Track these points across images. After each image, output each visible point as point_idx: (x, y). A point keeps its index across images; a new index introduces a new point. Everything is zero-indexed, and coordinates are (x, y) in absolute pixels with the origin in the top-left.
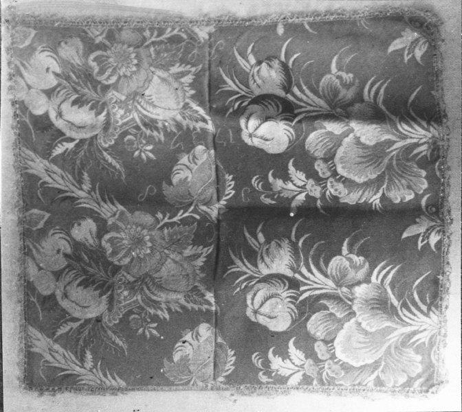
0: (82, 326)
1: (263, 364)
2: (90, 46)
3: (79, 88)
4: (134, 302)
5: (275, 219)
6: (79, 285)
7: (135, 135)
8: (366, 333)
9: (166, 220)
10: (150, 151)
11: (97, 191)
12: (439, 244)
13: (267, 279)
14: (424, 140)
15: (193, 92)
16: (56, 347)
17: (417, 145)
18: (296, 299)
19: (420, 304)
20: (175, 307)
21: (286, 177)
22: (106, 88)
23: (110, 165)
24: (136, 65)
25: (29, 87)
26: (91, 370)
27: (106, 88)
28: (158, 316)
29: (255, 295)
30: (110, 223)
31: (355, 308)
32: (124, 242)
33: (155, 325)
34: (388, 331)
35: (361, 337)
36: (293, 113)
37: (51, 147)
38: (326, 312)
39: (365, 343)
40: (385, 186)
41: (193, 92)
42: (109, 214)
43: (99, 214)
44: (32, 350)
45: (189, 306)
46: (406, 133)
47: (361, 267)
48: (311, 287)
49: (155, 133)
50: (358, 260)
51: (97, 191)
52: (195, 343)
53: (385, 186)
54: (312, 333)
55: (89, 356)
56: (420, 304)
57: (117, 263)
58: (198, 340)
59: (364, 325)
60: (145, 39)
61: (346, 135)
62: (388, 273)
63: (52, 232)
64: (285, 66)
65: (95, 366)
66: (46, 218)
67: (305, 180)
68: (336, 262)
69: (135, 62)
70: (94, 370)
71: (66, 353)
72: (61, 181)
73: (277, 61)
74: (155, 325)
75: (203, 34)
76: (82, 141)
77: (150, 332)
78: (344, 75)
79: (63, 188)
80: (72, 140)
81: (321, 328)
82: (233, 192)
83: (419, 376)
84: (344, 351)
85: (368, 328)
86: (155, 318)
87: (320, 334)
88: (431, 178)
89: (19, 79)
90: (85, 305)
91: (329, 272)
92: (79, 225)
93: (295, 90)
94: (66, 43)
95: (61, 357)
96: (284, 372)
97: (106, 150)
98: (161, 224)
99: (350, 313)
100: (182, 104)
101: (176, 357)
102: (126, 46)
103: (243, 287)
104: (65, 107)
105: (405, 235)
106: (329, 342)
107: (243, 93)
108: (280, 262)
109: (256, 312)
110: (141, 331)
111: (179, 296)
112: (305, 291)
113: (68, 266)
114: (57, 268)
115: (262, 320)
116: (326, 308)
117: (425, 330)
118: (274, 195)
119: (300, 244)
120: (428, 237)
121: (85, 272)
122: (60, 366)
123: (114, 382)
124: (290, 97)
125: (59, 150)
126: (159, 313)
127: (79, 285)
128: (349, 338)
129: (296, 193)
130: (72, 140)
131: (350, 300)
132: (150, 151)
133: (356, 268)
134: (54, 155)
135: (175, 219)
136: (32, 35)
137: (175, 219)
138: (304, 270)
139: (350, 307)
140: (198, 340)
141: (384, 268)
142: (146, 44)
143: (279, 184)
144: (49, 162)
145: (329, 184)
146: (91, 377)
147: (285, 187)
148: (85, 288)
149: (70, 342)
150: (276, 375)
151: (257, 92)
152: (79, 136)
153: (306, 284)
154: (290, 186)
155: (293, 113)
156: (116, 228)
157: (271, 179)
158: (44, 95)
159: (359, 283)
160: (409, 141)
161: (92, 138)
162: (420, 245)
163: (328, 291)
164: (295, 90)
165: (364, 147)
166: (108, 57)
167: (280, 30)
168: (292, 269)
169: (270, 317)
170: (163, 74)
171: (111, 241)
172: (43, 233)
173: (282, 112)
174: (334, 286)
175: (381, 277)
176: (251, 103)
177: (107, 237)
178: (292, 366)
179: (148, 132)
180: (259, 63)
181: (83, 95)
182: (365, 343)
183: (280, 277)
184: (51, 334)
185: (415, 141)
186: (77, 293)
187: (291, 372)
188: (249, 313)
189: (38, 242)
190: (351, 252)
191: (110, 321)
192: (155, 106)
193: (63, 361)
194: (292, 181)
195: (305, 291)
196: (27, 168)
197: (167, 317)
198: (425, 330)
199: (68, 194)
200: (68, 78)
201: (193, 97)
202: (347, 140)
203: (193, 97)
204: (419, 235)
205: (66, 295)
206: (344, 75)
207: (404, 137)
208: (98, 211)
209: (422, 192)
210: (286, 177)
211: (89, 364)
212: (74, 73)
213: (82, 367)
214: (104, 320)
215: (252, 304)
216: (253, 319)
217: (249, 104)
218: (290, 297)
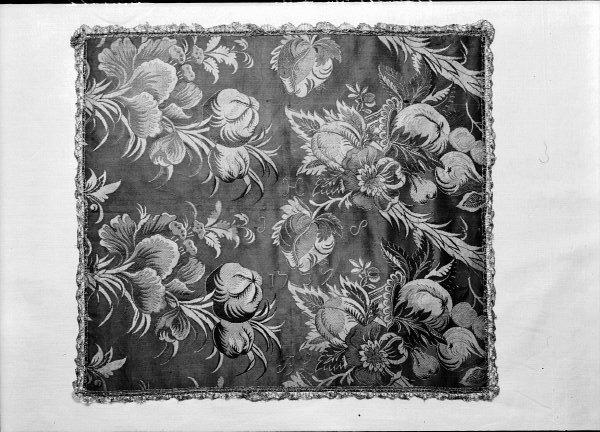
0: (424, 96)
1: (243, 57)
2: (407, 369)
3: (421, 329)
4: (370, 121)
5: (237, 194)
6: (425, 138)
7: (369, 282)
8: (149, 91)
9: (342, 200)
10: (354, 267)
11: (407, 230)
12: (87, 176)
13: (242, 141)
14: (101, 272)
15: (307, 323)
16: (448, 76)
17: (107, 268)
18: (213, 119)
19: (102, 118)
20: (330, 114)
21: (223, 241)
22: (394, 329)
23: (394, 254)
24: (361, 349)
25: (470, 329)
26: (415, 52)
27: (394, 329)
28: (347, 104)
29: (251, 122)
30: (397, 198)
31: (160, 113)
32: (384, 180)
33: (350, 96)
34: (129, 94)
35: (154, 86)
36: (215, 302)
37: (452, 271)
38: (187, 107)
39: (151, 82)
40: (136, 231)
41: (307, 323)
42: (397, 206)
43: (406, 207)
44: (477, 72)
45: (316, 117)
46: (117, 279)
47: (156, 156)
48: (199, 131)
49: (349, 284)
50: (159, 162)
51: (407, 230)
52: (311, 77)
53: (136, 231)
54: (197, 89)
55: (417, 66)
56: (102, 118)
57: (391, 159)
58: (309, 81)
59: (151, 97)
60: (352, 374)
61: (170, 278)
62: (129, 153)
63: (456, 189)
64: (221, 348)
65: (410, 56)
66: (461, 203)
67: (207, 239)
68: (179, 159)
69: (362, 353)
70: (411, 52)
71: (439, 70)
72: (444, 238)
73: (228, 353)
74: (350, 96)
75: (297, 380)
76: (421, 276)
77: (354, 87)
78: (168, 339)
79: (443, 232)
80: (434, 278)
81: (190, 93)
82: (274, 228)
83: (101, 50)
84: (167, 73)
85: (147, 94)
86: (350, 102)
87: (190, 87)
88: (95, 239)
89: (479, 335)
90: (420, 118)
91: (185, 148)
92: (427, 196)
93: (212, 326)
94: (430, 372)
95: (446, 66)
96: (222, 49)
97: (398, 269)
98: (347, 196)
99: (163, 108)
100: (319, 313)
101: (329, 63)
102: (370, 368)
103: (262, 134)
104: (437, 310)
105: (118, 184)
106: (182, 81)
107: (259, 324)
108: (230, 161)
109: (251, 106)
110: (365, 91)
111: (325, 127)
112: (205, 126)
113: (441, 156)
114: (450, 154)
115: (245, 99)
116: (185, 111)
117: (97, 94)
118: (236, 224)
119: (211, 174)
120: (98, 182)
121: (420, 150)
122: (445, 57)
123: (390, 38)
124: (217, 320)
125: (446, 268)
126: (346, 108)
127: (425, 138)
128: (165, 86)
129: (216, 225)
130: (434, 278)
131: (163, 120)
132: (354, 267)
133: (161, 154)
134: (450, 265)
135: (334, 200)
136: (465, 378)
137: (334, 200)
138: (207, 150)
139: (164, 114)
140: (309, 81)
141: (136, 154)
142: (351, 370)
143: (230, 235)
144: (454, 257)
145: (185, 234)
146: (414, 44)
147: (225, 232)
148: (419, 136)
149: (435, 81)
150: (230, 47)
151: (246, 325)
152: (425, 282)
153: (203, 134)
154: (220, 232)
155: (215, 302)
156: (393, 193)
157: (238, 239)
158: (456, 322)
159: (158, 137)
160: (114, 271)
161: (411, 280)
162: (105, 175)
163: (183, 127)
164: (212, 326)
165: (152, 266)
166: (388, 358)
167: (221, 382)
168: (218, 153)
169: (238, 101)
170: (335, 341)
171: (395, 180)
172: (464, 189)
173: (224, 303)
174: (180, 134)
175: (138, 145)
176: (253, 314)
177: (400, 185)
178: (215, 56)
179: (356, 285)
180: (244, 352)
181: (417, 322)
182: (151, 82)
183: (228, 144)
184: (457, 89)
185: (109, 271)
186: (428, 130)
187: (217, 51)
188: (257, 104)
189: (470, 180)
190: (165, 169)
191: (395, 101)
192: (348, 311)
193: (441, 62)
194: (218, 237)
195: (205, 126)
196: (478, 251)
197: (338, 104)
198: (97, 94)
199: (438, 226)
200: (431, 339)
201: (308, 318)
202: (169, 273)
203: (308, 318)
204: (106, 184)
205: (439, 128)
206: (168, 339)
207: (119, 274)
208: (407, 210)
209: (104, 226)
210: (223, 241)
211: (417, 59)
212: (423, 343)
213: (423, 55)
214: (401, 103)
215: (253, 114)
216: (253, 99)
217: (254, 312)
218: (218, 120)
